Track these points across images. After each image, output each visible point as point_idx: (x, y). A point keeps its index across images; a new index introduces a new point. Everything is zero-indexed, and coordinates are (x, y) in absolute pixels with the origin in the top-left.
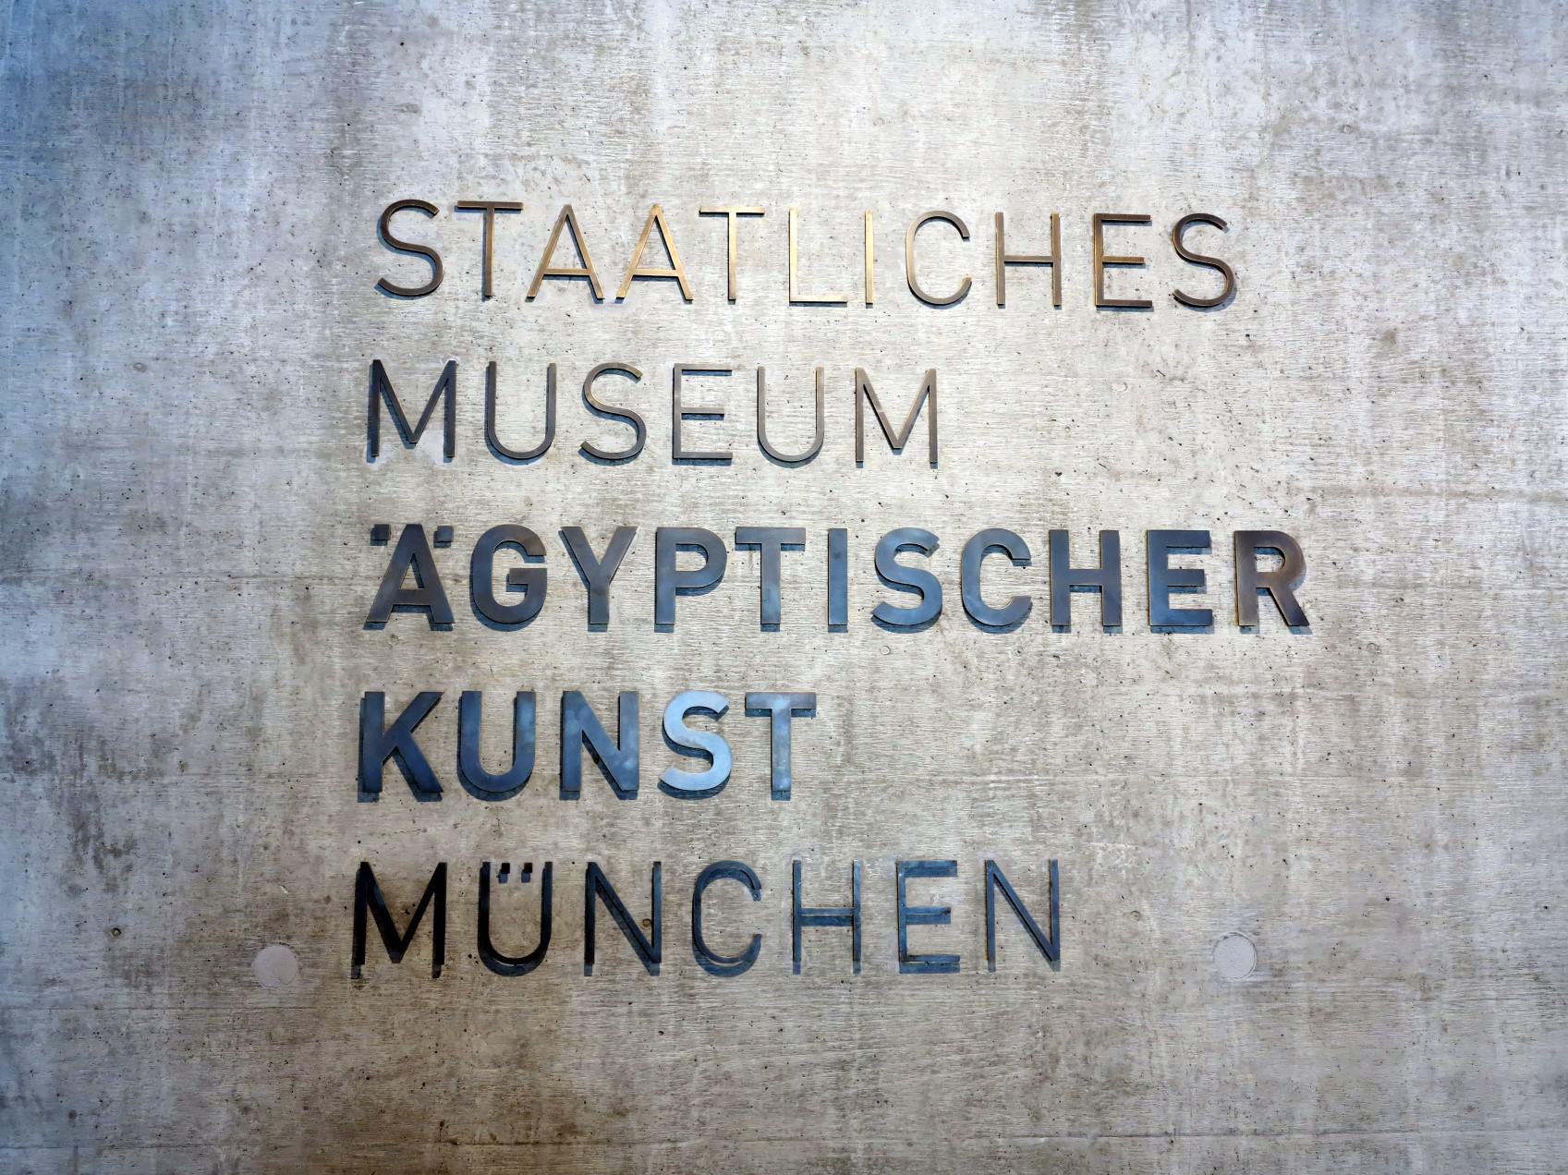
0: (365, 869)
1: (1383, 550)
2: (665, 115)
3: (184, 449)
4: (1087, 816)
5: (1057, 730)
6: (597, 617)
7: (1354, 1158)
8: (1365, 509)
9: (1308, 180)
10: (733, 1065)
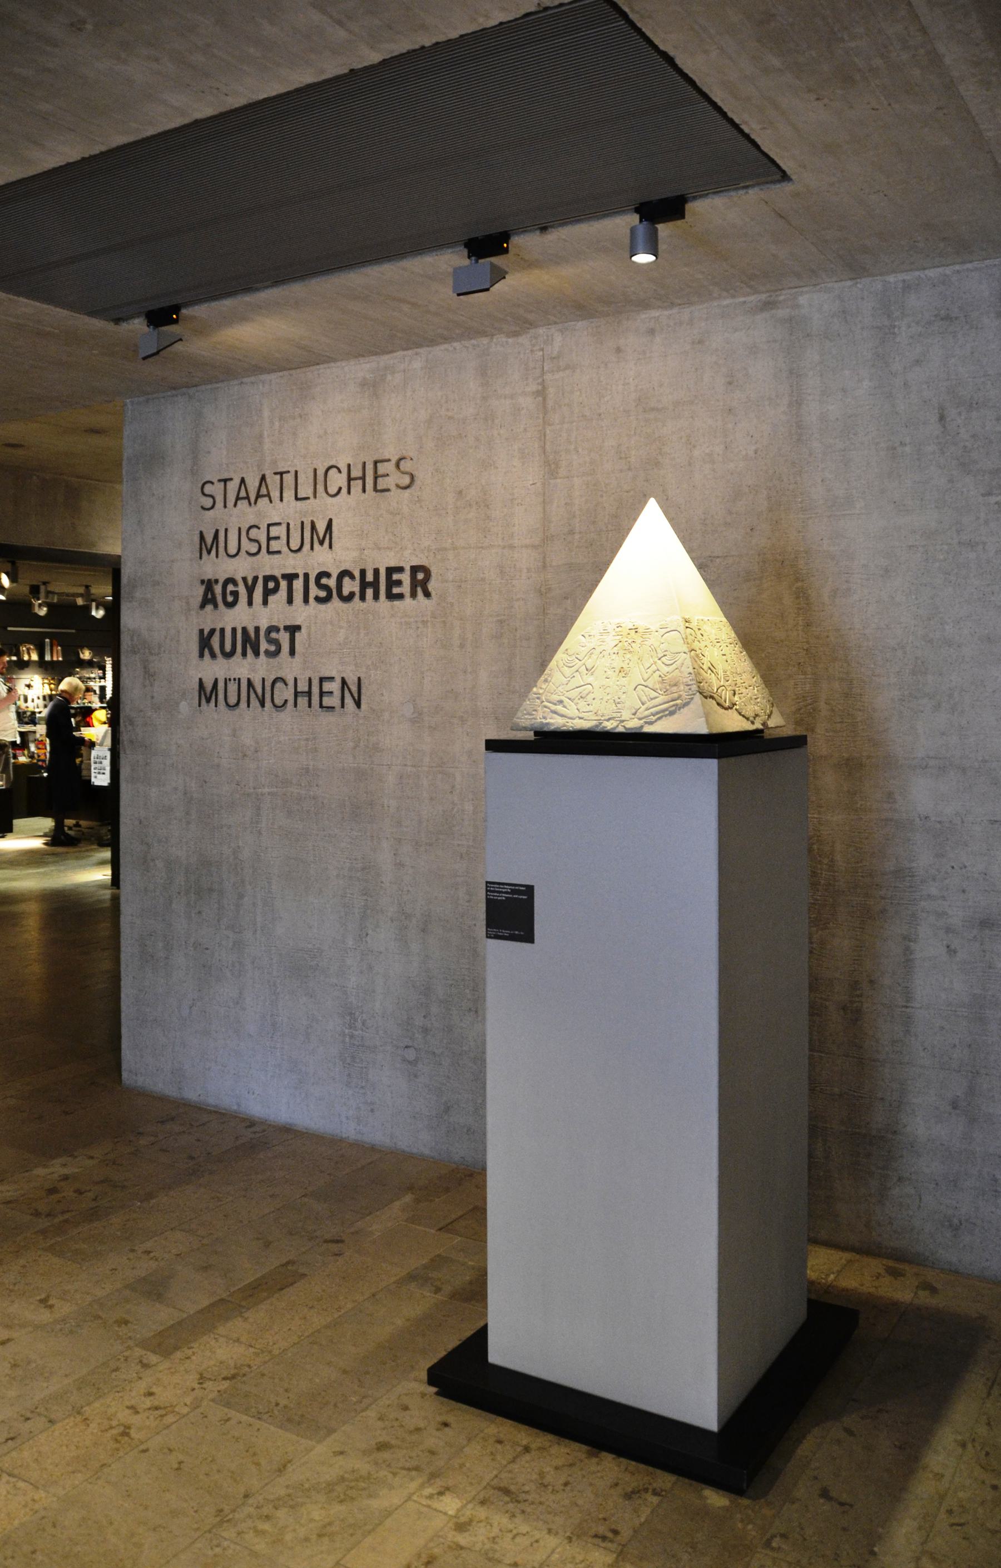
0: (200, 680)
1: (456, 569)
2: (267, 446)
3: (163, 561)
4: (370, 663)
5: (362, 635)
6: (250, 603)
7: (440, 776)
8: (450, 555)
9: (438, 439)
10: (282, 738)
